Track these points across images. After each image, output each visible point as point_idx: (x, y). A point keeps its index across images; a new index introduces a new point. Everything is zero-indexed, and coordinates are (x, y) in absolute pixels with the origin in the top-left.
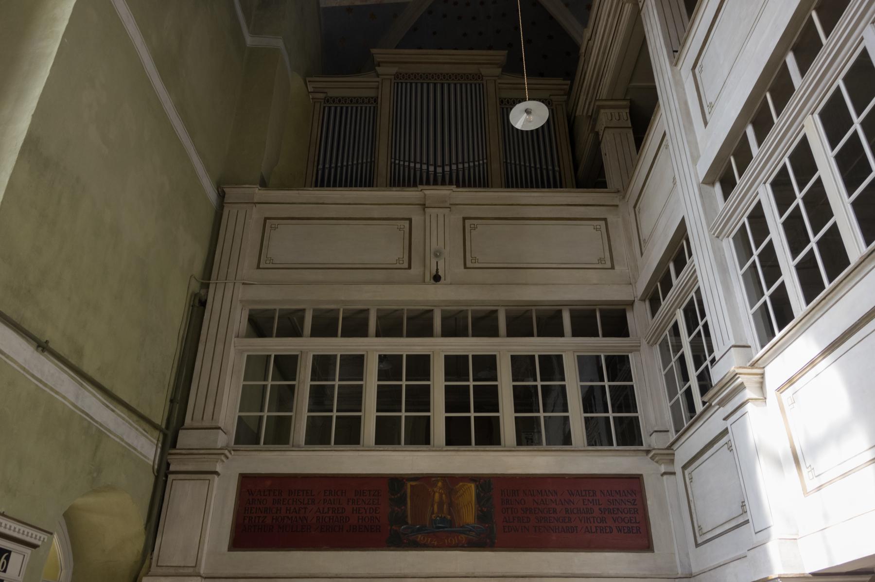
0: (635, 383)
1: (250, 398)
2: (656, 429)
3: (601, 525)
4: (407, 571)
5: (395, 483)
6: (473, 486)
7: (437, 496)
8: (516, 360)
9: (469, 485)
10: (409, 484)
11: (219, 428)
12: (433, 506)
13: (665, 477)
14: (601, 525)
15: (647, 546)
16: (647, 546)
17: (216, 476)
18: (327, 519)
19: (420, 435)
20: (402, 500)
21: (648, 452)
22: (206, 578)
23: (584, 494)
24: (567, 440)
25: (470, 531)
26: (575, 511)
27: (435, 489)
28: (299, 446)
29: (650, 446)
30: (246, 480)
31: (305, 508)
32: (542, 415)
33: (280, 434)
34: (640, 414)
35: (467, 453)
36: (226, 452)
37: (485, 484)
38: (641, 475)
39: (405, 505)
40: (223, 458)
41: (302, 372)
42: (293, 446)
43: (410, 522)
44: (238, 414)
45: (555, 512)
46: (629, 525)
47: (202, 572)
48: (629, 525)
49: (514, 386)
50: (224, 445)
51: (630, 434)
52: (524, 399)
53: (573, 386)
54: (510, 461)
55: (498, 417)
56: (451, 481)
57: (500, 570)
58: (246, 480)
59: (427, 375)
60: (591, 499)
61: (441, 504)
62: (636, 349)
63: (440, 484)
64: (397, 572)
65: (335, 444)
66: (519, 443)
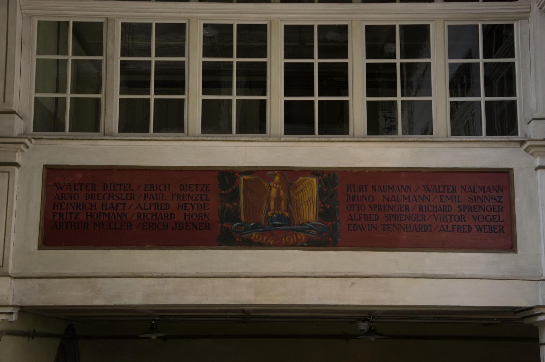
0: (517, 60)
1: (49, 76)
2: (536, 116)
3: (459, 223)
4: (239, 271)
5: (227, 177)
6: (315, 180)
7: (274, 191)
8: (372, 32)
9: (311, 179)
10: (242, 178)
11: (14, 113)
12: (269, 202)
13: (539, 171)
14: (459, 223)
15: (510, 246)
16: (510, 246)
17: (16, 168)
18: (149, 216)
19: (253, 122)
20: (234, 196)
21: (522, 142)
22: (15, 278)
23: (442, 189)
24: (427, 130)
25: (311, 229)
26: (430, 208)
27: (272, 184)
28: (111, 135)
29: (526, 135)
30: (52, 173)
31: (124, 204)
32: (399, 99)
33: (87, 120)
34: (519, 98)
35: (309, 144)
36: (26, 141)
37: (328, 177)
38: (511, 169)
39: (238, 201)
40: (22, 147)
41: (110, 44)
42: (105, 134)
43: (243, 219)
44: (34, 95)
45: (407, 208)
46: (492, 224)
47: (10, 272)
48: (492, 224)
49: (368, 65)
50: (22, 132)
51: (503, 122)
52: (379, 80)
53: (439, 63)
54: (359, 152)
55: (347, 102)
56: (290, 175)
57: (309, 270)
58: (52, 173)
59: (262, 51)
60: (449, 195)
61: (278, 200)
62: (525, 16)
63: (277, 178)
64: (229, 271)
65: (155, 131)
66: (455, 132)
